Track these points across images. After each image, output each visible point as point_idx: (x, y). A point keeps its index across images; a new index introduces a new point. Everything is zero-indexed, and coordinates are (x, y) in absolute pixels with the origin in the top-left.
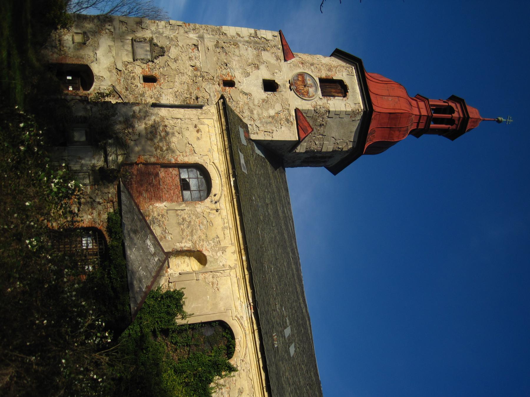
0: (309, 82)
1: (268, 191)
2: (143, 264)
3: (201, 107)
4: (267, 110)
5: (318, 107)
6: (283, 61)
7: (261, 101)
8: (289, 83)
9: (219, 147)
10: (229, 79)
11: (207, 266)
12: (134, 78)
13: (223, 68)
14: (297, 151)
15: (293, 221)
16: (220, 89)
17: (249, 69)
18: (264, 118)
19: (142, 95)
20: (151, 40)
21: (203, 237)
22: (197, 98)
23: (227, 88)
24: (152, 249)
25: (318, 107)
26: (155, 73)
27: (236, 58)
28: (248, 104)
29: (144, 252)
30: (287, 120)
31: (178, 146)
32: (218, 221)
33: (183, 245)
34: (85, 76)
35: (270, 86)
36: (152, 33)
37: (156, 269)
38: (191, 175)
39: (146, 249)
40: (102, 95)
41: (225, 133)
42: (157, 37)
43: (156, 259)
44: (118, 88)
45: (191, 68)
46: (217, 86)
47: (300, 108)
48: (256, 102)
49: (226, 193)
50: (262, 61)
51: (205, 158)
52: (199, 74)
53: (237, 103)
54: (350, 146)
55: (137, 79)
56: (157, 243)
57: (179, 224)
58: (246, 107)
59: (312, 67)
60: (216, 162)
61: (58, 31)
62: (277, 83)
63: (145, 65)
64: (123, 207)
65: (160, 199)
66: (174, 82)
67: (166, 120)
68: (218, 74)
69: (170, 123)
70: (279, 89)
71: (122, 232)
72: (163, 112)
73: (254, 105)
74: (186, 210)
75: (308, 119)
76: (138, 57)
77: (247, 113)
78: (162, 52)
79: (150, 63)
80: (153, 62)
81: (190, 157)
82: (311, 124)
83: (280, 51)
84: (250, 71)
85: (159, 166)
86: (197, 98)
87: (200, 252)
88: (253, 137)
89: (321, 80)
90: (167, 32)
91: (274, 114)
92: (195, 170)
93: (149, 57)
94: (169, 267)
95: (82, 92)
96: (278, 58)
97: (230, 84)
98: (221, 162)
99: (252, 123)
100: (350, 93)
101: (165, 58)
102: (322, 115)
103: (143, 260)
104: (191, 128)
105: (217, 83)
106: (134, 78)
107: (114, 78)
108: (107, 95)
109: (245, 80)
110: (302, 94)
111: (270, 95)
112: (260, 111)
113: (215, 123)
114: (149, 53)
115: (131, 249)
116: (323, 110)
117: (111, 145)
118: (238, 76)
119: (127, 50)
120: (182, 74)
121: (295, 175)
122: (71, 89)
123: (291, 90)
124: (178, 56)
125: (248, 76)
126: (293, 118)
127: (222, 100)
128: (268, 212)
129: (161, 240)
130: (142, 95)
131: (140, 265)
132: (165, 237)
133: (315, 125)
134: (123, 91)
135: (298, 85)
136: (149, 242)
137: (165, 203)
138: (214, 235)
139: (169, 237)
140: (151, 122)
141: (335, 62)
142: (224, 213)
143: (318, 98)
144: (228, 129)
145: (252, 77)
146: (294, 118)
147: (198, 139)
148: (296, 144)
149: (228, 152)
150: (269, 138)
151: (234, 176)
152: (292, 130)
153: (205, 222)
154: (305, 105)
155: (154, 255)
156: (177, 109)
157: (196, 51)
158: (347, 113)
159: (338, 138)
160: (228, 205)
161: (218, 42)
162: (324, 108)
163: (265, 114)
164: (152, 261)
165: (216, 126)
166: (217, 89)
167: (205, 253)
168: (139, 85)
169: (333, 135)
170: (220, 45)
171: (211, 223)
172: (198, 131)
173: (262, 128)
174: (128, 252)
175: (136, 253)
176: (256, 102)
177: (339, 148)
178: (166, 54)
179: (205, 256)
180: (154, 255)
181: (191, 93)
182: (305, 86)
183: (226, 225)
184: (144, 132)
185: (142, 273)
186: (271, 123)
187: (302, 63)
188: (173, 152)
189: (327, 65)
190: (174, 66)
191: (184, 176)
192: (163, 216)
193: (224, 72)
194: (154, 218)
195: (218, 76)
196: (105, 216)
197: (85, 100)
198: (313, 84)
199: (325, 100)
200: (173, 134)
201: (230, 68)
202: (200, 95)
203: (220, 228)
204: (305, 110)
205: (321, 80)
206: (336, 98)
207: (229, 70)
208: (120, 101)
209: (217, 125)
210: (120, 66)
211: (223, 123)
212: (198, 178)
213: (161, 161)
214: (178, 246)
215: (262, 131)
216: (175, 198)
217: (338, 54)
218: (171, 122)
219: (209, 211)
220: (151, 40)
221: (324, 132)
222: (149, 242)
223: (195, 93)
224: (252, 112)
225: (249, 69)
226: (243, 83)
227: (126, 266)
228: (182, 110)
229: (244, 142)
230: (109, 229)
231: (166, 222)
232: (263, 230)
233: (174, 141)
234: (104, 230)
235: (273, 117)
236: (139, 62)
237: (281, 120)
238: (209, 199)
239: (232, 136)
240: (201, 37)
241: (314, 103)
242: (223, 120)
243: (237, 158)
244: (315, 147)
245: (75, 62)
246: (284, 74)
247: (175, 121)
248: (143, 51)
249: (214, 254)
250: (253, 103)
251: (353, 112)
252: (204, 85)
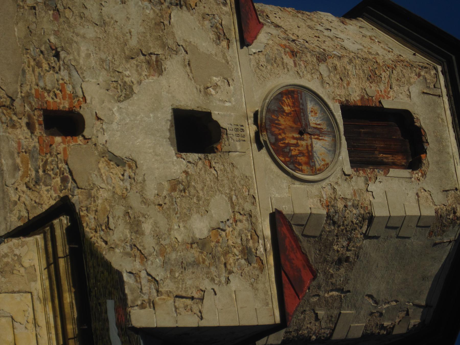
0: (314, 119)
4: (185, 217)
5: (340, 205)
6: (235, 45)
7: (166, 185)
8: (256, 122)
10: (65, 105)
13: (45, 66)
16: (34, 143)
17: (130, 73)
18: (174, 249)
23: (58, 139)
25: (340, 205)
27: (91, 32)
28: (124, 197)
30: (248, 254)
35: (195, 132)
46: (22, 133)
47: (286, 209)
48: (151, 191)
50: (170, 42)
53: (90, 196)
54: (415, 321)
58: (119, 211)
59: (323, 68)
62: (216, 123)
68: (26, 88)
70: (225, 144)
73: (145, 201)
75: (305, 244)
77: (120, 232)
82: (312, 258)
83: (226, 9)
84: (135, 78)
89: (348, 110)
91: (205, 233)
96: (220, 35)
99: (137, 265)
100: (430, 157)
102: (347, 232)
105: (25, 120)
109: (117, 113)
110: (293, 162)
111: (196, 164)
112: (163, 223)
113: (39, 306)
116: (352, 215)
118: (94, 96)
123: (260, 147)
125: (127, 97)
126: (264, 248)
127: (65, 220)
133: (325, 260)
135: (282, 128)
143: (339, 174)
145: (141, 100)
146: (269, 245)
150: (189, 321)
152: (260, 286)
154: (302, 199)
158: (421, 223)
162: (355, 206)
163: (179, 234)
165: (42, 321)
166: (24, 142)
169: (372, 289)
173: (168, 286)
176: (151, 191)
177: (382, 327)
182: (301, 133)
186: (196, 263)
187: (293, 54)
189: (365, 60)
193: (49, 79)
195: (28, 95)
198: (324, 127)
199: (358, 182)
201: (67, 67)
204: (300, 216)
205: (348, 110)
206: (393, 172)
207: (64, 73)
209: (45, 315)
211: (67, 309)
215: (168, 294)
221: (347, 280)
224: (135, 225)
225: (130, 73)
226: (111, 122)
235: (202, 244)
237: (226, 254)
241: (329, 191)
242: (68, 298)
244: (314, 327)
246: (238, 95)
250: (142, 193)
251: (439, 217)
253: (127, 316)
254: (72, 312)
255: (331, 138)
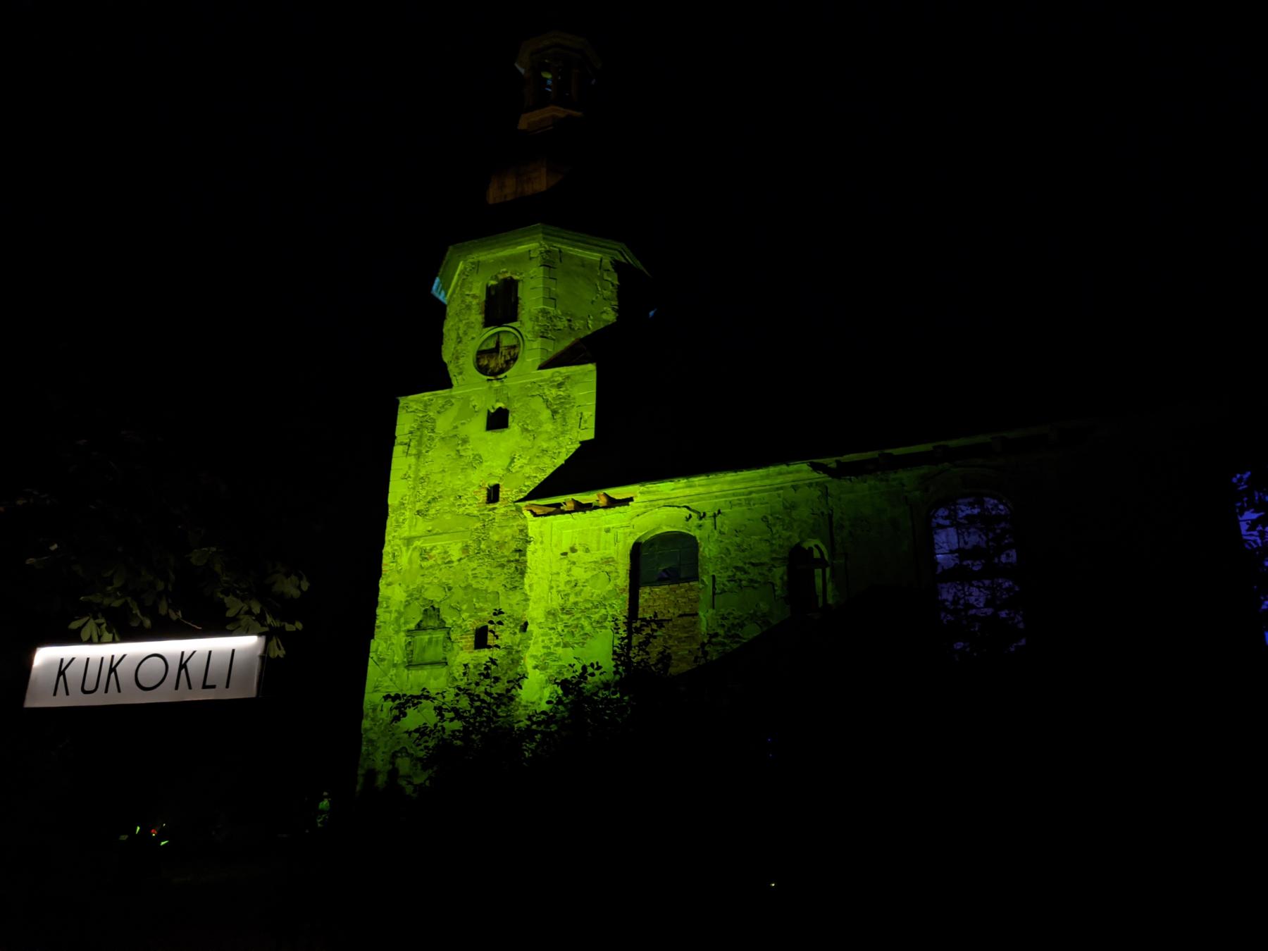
9: (703, 482)
10: (485, 492)
36: (397, 632)
42: (406, 623)
63: (455, 646)
78: (432, 611)
89: (488, 323)
96: (449, 402)
97: (493, 494)
112: (544, 436)
118: (479, 479)
139: (764, 607)
161: (419, 512)
181: (509, 561)
205: (488, 323)
235: (554, 412)
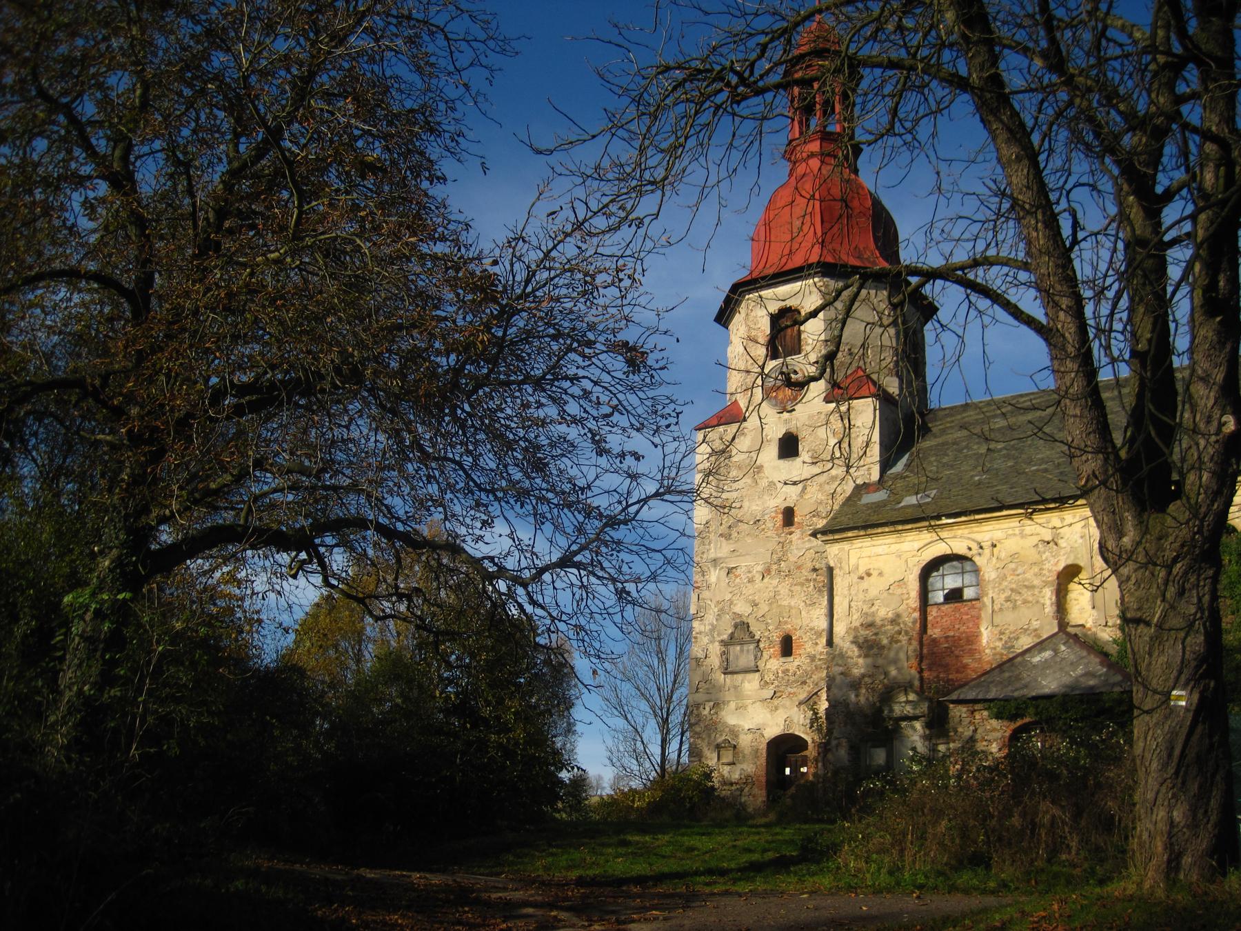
1: (967, 447)
2: (1067, 669)
3: (830, 570)
10: (780, 516)
11: (1082, 564)
12: (786, 672)
14: (897, 391)
15: (1021, 396)
16: (798, 531)
19: (813, 658)
20: (724, 643)
21: (1036, 569)
22: (815, 570)
24: (1047, 654)
26: (776, 637)
29: (1049, 667)
31: (893, 606)
32: (1010, 545)
33: (1048, 602)
34: (784, 748)
35: (789, 446)
36: (712, 642)
37: (1077, 648)
38: (939, 585)
39: (1046, 664)
40: (815, 718)
41: (870, 531)
43: (1063, 648)
44: (803, 696)
45: (766, 580)
46: (794, 537)
49: (966, 531)
51: (910, 565)
52: (775, 567)
55: (787, 666)
56: (1040, 646)
57: (1015, 607)
60: (917, 545)
61: (717, 785)
64: (980, 697)
65: (978, 635)
66: (790, 607)
67: (853, 625)
69: (856, 619)
70: (794, 430)
71: (1016, 699)
72: (840, 629)
74: (993, 596)
76: (753, 664)
78: (742, 626)
79: (762, 645)
80: (759, 641)
81: (911, 587)
85: (925, 637)
86: (815, 570)
87: (1059, 575)
88: (875, 476)
90: (710, 618)
92: (931, 580)
93: (752, 647)
94: (1083, 626)
95: (811, 752)
97: (788, 516)
98: (917, 538)
101: (751, 621)
103: (1061, 669)
104: (865, 584)
106: (786, 672)
107: (787, 702)
108: (816, 714)
114: (745, 647)
115: (1043, 687)
117: (891, 711)
118: (776, 502)
119: (742, 682)
120: (776, 593)
121: (945, 392)
122: (804, 770)
124: (747, 601)
128: (1001, 450)
129: (1038, 636)
130: (813, 658)
131: (1067, 673)
132: (1036, 630)
134: (807, 688)
136: (1036, 659)
137: (982, 629)
138: (1034, 551)
139: (1035, 624)
140: (856, 651)
141: (738, 326)
142: (998, 535)
144: (865, 527)
147: (881, 574)
148: (885, 399)
149: (900, 527)
151: (938, 517)
153: (1012, 566)
155: (1056, 651)
156: (835, 607)
157: (738, 572)
159: (871, 324)
160: (985, 528)
164: (1065, 655)
167: (1061, 567)
168: (796, 663)
170: (727, 531)
171: (1014, 556)
172: (869, 575)
174: (1047, 691)
175: (1049, 679)
178: (745, 620)
179: (1067, 567)
180: (1056, 651)
183: (1017, 531)
184: (869, 660)
185: (1080, 670)
188: (898, 616)
190: (764, 608)
191: (939, 597)
192: (1002, 633)
193: (769, 525)
194: (1004, 647)
196: (995, 723)
197: (824, 748)
200: (873, 614)
202: (809, 565)
203: (1022, 542)
208: (824, 696)
209: (858, 543)
210: (768, 693)
212: (943, 575)
213: (915, 634)
214: (1049, 609)
216: (974, 613)
217: (724, 317)
218: (855, 617)
219: (994, 560)
220: (724, 643)
222: (1036, 659)
223: (806, 573)
225: (763, 483)
227: (1065, 695)
228: (836, 599)
229: (881, 496)
230: (1012, 718)
231: (1012, 628)
232: (1030, 462)
233: (883, 612)
234: (1013, 726)
236: (761, 664)
238: (976, 559)
239: (874, 519)
240: (715, 561)
242: (850, 534)
243: (910, 510)
245: (763, 760)
247: (853, 610)
248: (743, 656)
249: (1062, 552)
252: (792, 559)
253: (873, 484)
254: (855, 533)
255: (777, 174)
